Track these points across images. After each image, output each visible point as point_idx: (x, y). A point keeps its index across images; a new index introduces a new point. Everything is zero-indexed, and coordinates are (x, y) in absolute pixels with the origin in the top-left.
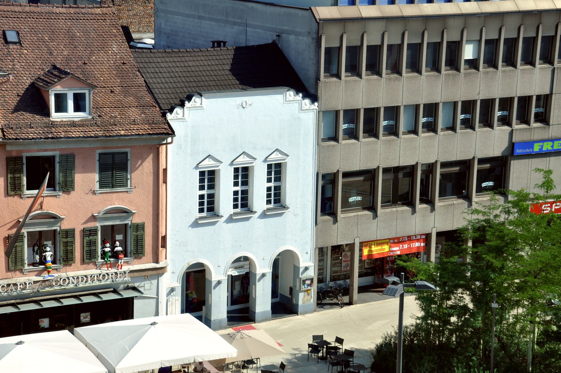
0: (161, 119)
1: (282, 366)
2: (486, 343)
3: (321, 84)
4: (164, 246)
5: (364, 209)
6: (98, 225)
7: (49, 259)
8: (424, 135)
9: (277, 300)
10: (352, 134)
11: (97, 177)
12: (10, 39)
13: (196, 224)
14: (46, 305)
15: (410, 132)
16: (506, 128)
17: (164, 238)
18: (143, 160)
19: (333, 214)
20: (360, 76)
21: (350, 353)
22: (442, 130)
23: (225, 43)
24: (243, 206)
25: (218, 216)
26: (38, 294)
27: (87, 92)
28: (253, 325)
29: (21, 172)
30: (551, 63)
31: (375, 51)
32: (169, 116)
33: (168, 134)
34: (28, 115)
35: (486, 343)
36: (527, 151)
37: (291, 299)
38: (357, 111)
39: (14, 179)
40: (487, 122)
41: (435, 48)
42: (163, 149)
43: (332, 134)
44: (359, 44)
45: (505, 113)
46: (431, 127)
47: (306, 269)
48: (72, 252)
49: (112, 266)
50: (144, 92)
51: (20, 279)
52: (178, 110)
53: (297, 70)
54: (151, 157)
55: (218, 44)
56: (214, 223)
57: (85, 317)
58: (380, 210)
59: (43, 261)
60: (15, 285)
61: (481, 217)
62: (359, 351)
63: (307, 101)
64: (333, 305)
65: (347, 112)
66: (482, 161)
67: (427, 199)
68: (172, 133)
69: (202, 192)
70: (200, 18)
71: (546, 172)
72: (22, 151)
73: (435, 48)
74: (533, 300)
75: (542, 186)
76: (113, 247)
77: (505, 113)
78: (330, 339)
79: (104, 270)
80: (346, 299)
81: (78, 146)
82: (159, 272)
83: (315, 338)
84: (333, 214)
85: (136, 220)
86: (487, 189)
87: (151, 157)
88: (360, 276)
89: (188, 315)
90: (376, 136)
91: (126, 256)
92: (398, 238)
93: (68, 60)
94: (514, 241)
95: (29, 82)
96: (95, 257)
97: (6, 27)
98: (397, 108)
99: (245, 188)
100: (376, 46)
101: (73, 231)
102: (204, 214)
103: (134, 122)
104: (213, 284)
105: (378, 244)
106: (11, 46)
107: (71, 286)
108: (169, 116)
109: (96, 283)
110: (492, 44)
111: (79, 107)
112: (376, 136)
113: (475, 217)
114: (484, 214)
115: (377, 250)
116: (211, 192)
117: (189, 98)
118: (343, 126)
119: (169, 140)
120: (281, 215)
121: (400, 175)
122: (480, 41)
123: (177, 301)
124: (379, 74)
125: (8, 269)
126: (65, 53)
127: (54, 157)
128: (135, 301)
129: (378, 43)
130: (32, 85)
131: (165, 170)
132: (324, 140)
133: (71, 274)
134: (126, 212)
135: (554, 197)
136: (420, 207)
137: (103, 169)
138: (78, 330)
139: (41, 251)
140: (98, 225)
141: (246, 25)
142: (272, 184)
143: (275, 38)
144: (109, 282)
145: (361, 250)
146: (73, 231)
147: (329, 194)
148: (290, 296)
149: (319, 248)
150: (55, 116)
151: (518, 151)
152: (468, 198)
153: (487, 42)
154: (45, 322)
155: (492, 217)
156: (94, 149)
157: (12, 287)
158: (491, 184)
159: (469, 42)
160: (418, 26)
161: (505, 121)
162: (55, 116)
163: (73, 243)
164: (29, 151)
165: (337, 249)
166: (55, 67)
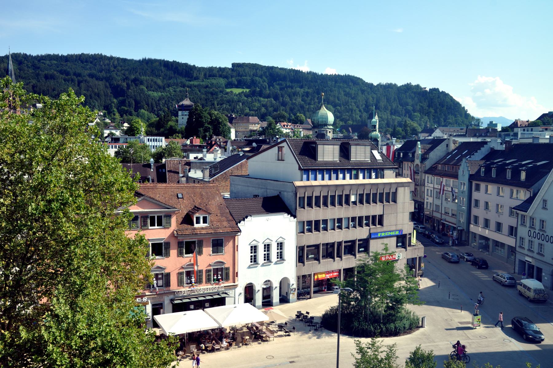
0: (236, 226)
1: (286, 324)
2: (365, 312)
3: (297, 211)
4: (237, 276)
5: (402, 248)
6: (212, 268)
7: (193, 281)
8: (337, 230)
9: (281, 297)
10: (310, 230)
11: (211, 249)
12: (179, 197)
13: (249, 267)
14: (193, 300)
15: (332, 229)
16: (368, 227)
17: (237, 273)
18: (229, 242)
19: (303, 262)
20: (312, 208)
21: (312, 318)
22: (344, 228)
23: (258, 196)
24: (281, 258)
25: (258, 264)
26: (189, 295)
27: (208, 216)
28: (272, 307)
29: (183, 247)
30: (383, 203)
31: (317, 198)
32: (239, 224)
33: (239, 232)
34: (186, 225)
35: (365, 312)
36: (376, 236)
37: (287, 297)
38: (312, 221)
39: (180, 250)
40: (361, 225)
41: (340, 197)
42: (236, 237)
43: (302, 231)
44: (311, 195)
45: (367, 222)
46: (340, 227)
47: (293, 285)
48: (202, 279)
49: (217, 284)
50: (229, 215)
51: (182, 289)
52: (242, 222)
53: (287, 205)
54: (232, 240)
55: (256, 196)
56: (257, 267)
57: (207, 305)
58: (321, 260)
59: (191, 283)
60: (181, 292)
61: (362, 262)
62: (316, 317)
63: (292, 218)
64: (303, 299)
65: (308, 222)
66: (359, 240)
67: (339, 256)
68: (240, 231)
69: (252, 254)
70: (248, 186)
71: (385, 244)
72: (184, 239)
73: (340, 197)
74: (382, 294)
75: (383, 250)
76: (217, 277)
77: (367, 222)
78: (304, 312)
79: (214, 286)
80: (308, 296)
81: (204, 237)
82: (235, 286)
83: (298, 312)
84: (303, 262)
85: (226, 266)
86: (361, 251)
87: (232, 240)
88: (314, 287)
89: (248, 304)
90: (319, 231)
91: (222, 280)
92: (328, 272)
93: (200, 204)
94: (375, 271)
95: (186, 213)
96: (211, 281)
97: (178, 192)
98: (327, 220)
99: (281, 251)
100: (310, 197)
101: (202, 270)
102: (253, 263)
103: (226, 227)
104: (256, 291)
105: (321, 274)
106: (180, 199)
107: (202, 292)
108: (239, 224)
109: (211, 291)
110: (361, 196)
111: (205, 221)
112: (319, 231)
113: (360, 262)
114: (363, 261)
115: (321, 277)
116: (268, 252)
117: (247, 217)
118: (306, 227)
119: (239, 234)
120: (282, 263)
121: (329, 247)
122: (357, 194)
123: (242, 298)
124: (320, 207)
125: (178, 286)
126: (199, 201)
127: (195, 241)
128: (226, 298)
129: (319, 195)
130: (187, 214)
131: (237, 246)
132: (299, 233)
133: (202, 287)
134: (222, 263)
135: (389, 254)
136: (336, 259)
137: (213, 246)
138: (205, 309)
139: (190, 278)
140: (212, 268)
141: (267, 189)
142: (253, 254)
143: (278, 193)
144: (216, 291)
145: (314, 276)
146: (202, 270)
147: (301, 255)
148: (286, 295)
149: (298, 277)
150: (196, 225)
151: (373, 236)
152: (355, 255)
153: (359, 194)
154: (192, 307)
155: (366, 262)
156: (210, 238)
157: (180, 293)
158: (363, 249)
159: (353, 194)
160: (333, 189)
161: (367, 225)
162: (196, 225)
163: (202, 275)
164: (186, 239)
165: (304, 277)
166: (195, 207)
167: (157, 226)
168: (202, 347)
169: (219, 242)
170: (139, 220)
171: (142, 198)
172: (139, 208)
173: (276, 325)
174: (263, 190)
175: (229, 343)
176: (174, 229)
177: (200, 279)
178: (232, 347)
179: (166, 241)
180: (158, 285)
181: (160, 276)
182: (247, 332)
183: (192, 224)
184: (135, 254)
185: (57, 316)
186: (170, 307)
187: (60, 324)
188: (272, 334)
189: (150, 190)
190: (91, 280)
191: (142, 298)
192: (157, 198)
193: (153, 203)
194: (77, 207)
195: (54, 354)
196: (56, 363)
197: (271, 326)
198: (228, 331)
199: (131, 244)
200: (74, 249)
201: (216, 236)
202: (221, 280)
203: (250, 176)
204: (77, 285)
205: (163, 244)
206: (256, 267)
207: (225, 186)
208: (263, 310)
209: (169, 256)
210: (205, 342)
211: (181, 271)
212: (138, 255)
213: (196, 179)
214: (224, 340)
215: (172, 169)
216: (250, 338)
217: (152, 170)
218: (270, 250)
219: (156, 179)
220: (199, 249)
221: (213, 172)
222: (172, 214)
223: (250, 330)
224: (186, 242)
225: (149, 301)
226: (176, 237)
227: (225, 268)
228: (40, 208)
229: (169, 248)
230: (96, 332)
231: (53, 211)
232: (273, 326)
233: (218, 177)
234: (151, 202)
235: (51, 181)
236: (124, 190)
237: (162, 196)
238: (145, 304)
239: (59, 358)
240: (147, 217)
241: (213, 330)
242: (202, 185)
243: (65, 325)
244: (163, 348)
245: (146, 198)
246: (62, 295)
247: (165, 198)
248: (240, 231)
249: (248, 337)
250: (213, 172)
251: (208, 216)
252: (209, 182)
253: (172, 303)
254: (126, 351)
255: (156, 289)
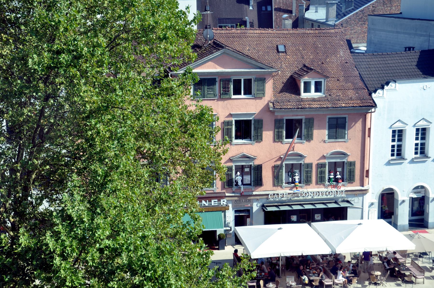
0: (368, 97)
4: (367, 176)
6: (327, 161)
7: (297, 180)
11: (326, 132)
12: (280, 50)
13: (389, 163)
14: (295, 208)
17: (368, 171)
23: (413, 48)
26: (290, 200)
27: (323, 80)
28: (427, 230)
29: (282, 128)
32: (373, 95)
33: (372, 106)
34: (288, 95)
39: (278, 132)
42: (368, 115)
48: (311, 177)
49: (334, 187)
51: (280, 191)
52: (379, 91)
57: (318, 216)
59: (293, 182)
60: (278, 194)
72: (284, 116)
76: (335, 175)
79: (330, 189)
82: (364, 192)
85: (350, 159)
89: (382, 220)
91: (343, 181)
93: (312, 61)
96: (324, 181)
102: (418, 156)
103: (351, 99)
104: (399, 202)
106: (281, 54)
107: (310, 197)
109: (325, 197)
117: (387, 84)
119: (373, 110)
123: (375, 211)
126: (311, 57)
127: (301, 120)
128: (348, 209)
130: (291, 77)
131: (370, 129)
138: (313, 224)
140: (327, 161)
141: (430, 36)
142: (395, 143)
144: (332, 196)
150: (304, 95)
154: (294, 218)
156: (325, 115)
157: (276, 196)
163: (311, 171)
164: (287, 116)
166: (305, 66)
167: (244, 94)
168: (304, 280)
169: (339, 122)
170: (217, 84)
171: (222, 51)
172: (217, 66)
173: (429, 258)
174: (422, 38)
175: (347, 278)
176: (269, 99)
177: (307, 177)
178: (352, 286)
179: (257, 118)
180: (244, 183)
181: (247, 170)
182: (379, 264)
183: (298, 93)
184: (192, 136)
185: (70, 217)
186: (262, 216)
187: (71, 230)
188: (421, 272)
189: (236, 39)
190: (120, 170)
191: (219, 200)
192: (246, 52)
193: (238, 59)
194: (98, 62)
195: (62, 271)
196: (65, 283)
197: (421, 259)
198: (348, 259)
199: (187, 120)
200: (96, 124)
201: (335, 112)
202: (340, 181)
203: (403, 15)
204: (99, 176)
205: (253, 122)
206: (401, 163)
207: (360, 33)
208: (411, 232)
209: (262, 140)
210: (309, 272)
211: (322, 161)
212: (196, 137)
213: (316, 21)
214: (340, 273)
215: (282, 7)
216: (383, 275)
217: (251, 8)
218: (403, 140)
219: (256, 23)
220: (308, 131)
221: (343, 10)
222: (266, 77)
223: (383, 262)
224: (286, 120)
225: (230, 205)
226: (272, 112)
227: (348, 162)
228: (44, 61)
229: (261, 128)
230: (123, 244)
231: (61, 67)
232: (424, 260)
233: (349, 18)
234: (235, 57)
235: (59, 21)
236: (168, 38)
237: (254, 49)
238: (224, 210)
239: (68, 277)
240: (229, 81)
241: (323, 256)
242: (317, 32)
243: (79, 232)
244: (224, 275)
245: (228, 51)
246: (78, 189)
247: (258, 51)
248: (374, 105)
249: (378, 273)
250: (343, 10)
251: (323, 80)
252: (335, 25)
253: (264, 210)
254: (163, 274)
255: (240, 188)
